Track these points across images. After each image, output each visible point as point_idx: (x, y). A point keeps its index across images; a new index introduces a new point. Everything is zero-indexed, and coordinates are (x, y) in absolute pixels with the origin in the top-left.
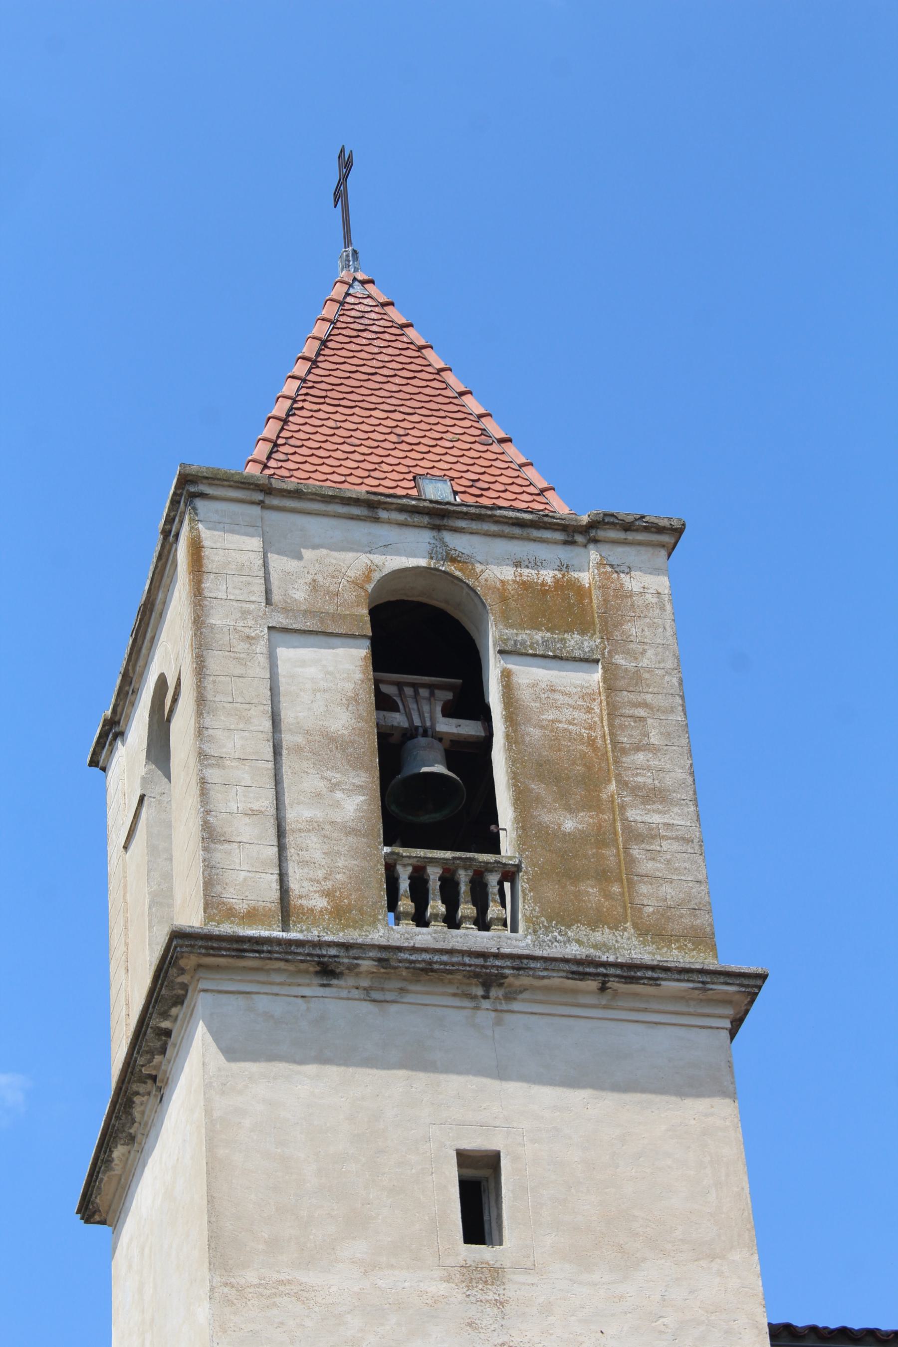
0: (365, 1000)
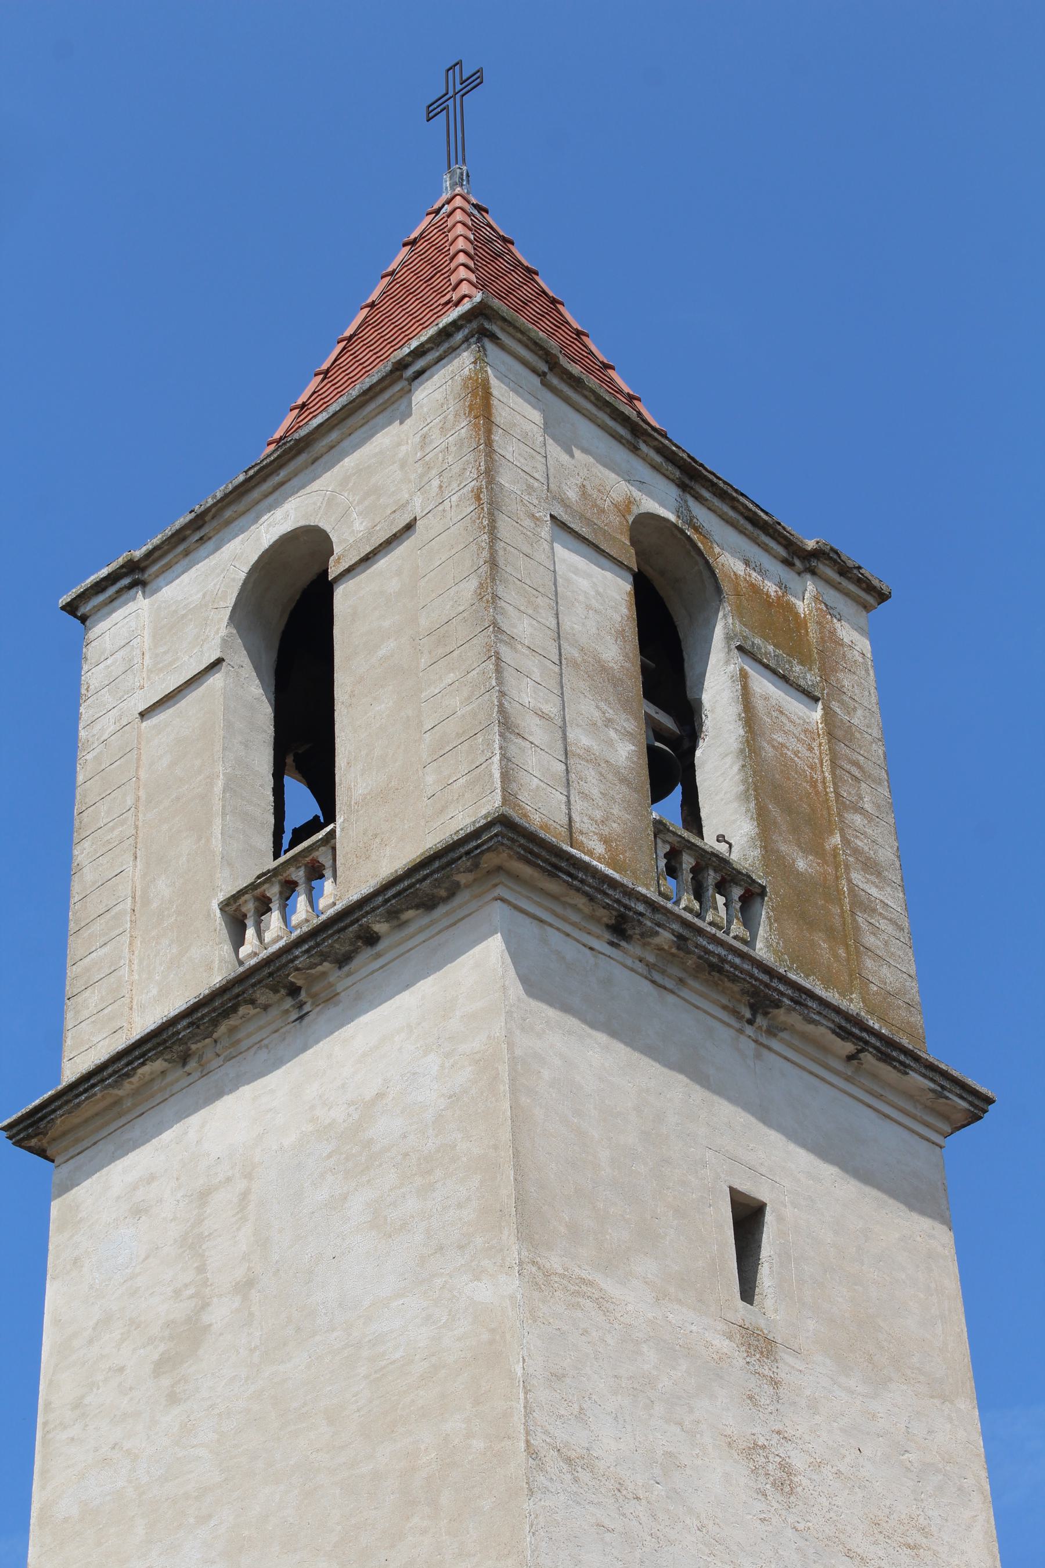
0: (646, 978)
